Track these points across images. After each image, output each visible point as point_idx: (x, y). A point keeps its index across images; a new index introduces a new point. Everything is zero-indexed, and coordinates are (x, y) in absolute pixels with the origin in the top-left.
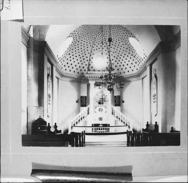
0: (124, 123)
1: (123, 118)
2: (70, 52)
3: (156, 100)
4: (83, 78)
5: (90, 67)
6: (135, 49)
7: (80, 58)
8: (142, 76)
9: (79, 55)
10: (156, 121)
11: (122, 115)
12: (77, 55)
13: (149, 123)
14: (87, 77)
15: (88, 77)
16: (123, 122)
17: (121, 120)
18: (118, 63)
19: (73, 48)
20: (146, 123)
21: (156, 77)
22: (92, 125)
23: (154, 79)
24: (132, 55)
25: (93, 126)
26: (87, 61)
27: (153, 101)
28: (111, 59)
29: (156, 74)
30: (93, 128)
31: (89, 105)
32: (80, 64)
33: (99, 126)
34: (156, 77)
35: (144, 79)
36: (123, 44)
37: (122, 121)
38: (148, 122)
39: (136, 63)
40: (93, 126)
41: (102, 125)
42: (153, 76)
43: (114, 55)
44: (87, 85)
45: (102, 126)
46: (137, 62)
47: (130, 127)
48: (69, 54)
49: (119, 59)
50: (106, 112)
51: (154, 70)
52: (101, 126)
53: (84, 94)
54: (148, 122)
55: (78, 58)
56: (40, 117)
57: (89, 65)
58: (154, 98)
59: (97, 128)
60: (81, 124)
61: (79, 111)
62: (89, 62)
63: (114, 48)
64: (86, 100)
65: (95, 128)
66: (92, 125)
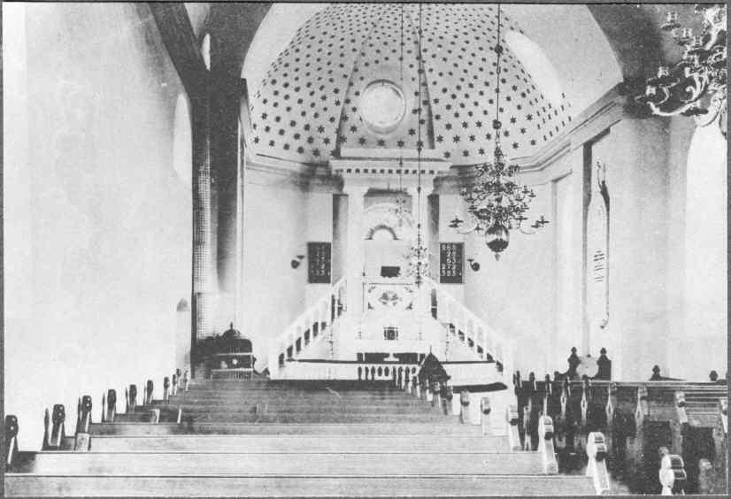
0: (480, 350)
1: (475, 330)
2: (275, 76)
3: (603, 273)
4: (321, 171)
5: (347, 125)
6: (527, 70)
7: (312, 94)
8: (554, 171)
9: (309, 85)
10: (713, 369)
11: (470, 321)
12: (302, 82)
13: (579, 354)
14: (337, 171)
15: (342, 170)
16: (475, 348)
17: (460, 333)
18: (457, 115)
19: (290, 59)
20: (569, 354)
21: (604, 192)
22: (360, 355)
23: (597, 199)
24: (515, 88)
25: (360, 360)
26: (338, 103)
27: (592, 274)
28: (432, 97)
29: (603, 182)
30: (363, 366)
31: (342, 280)
32: (309, 118)
33: (386, 359)
34: (604, 192)
35: (560, 184)
36: (481, 49)
37: (471, 344)
38: (574, 350)
39: (530, 118)
40: (360, 360)
41: (396, 355)
42: (596, 188)
43: (442, 82)
44: (331, 197)
45: (397, 360)
46: (535, 116)
47: (504, 365)
48: (274, 82)
49: (460, 98)
50: (410, 307)
51: (599, 167)
52: (391, 358)
53: (323, 235)
54: (574, 350)
55: (304, 93)
56: (231, 326)
57: (344, 118)
58: (596, 263)
59: (377, 366)
60: (312, 349)
61: (299, 305)
62: (343, 110)
63: (445, 59)
64: (328, 257)
65: (370, 366)
66: (360, 355)
